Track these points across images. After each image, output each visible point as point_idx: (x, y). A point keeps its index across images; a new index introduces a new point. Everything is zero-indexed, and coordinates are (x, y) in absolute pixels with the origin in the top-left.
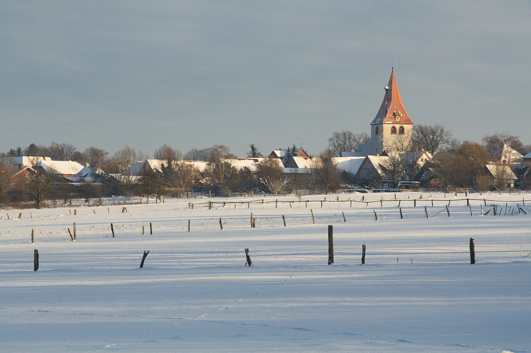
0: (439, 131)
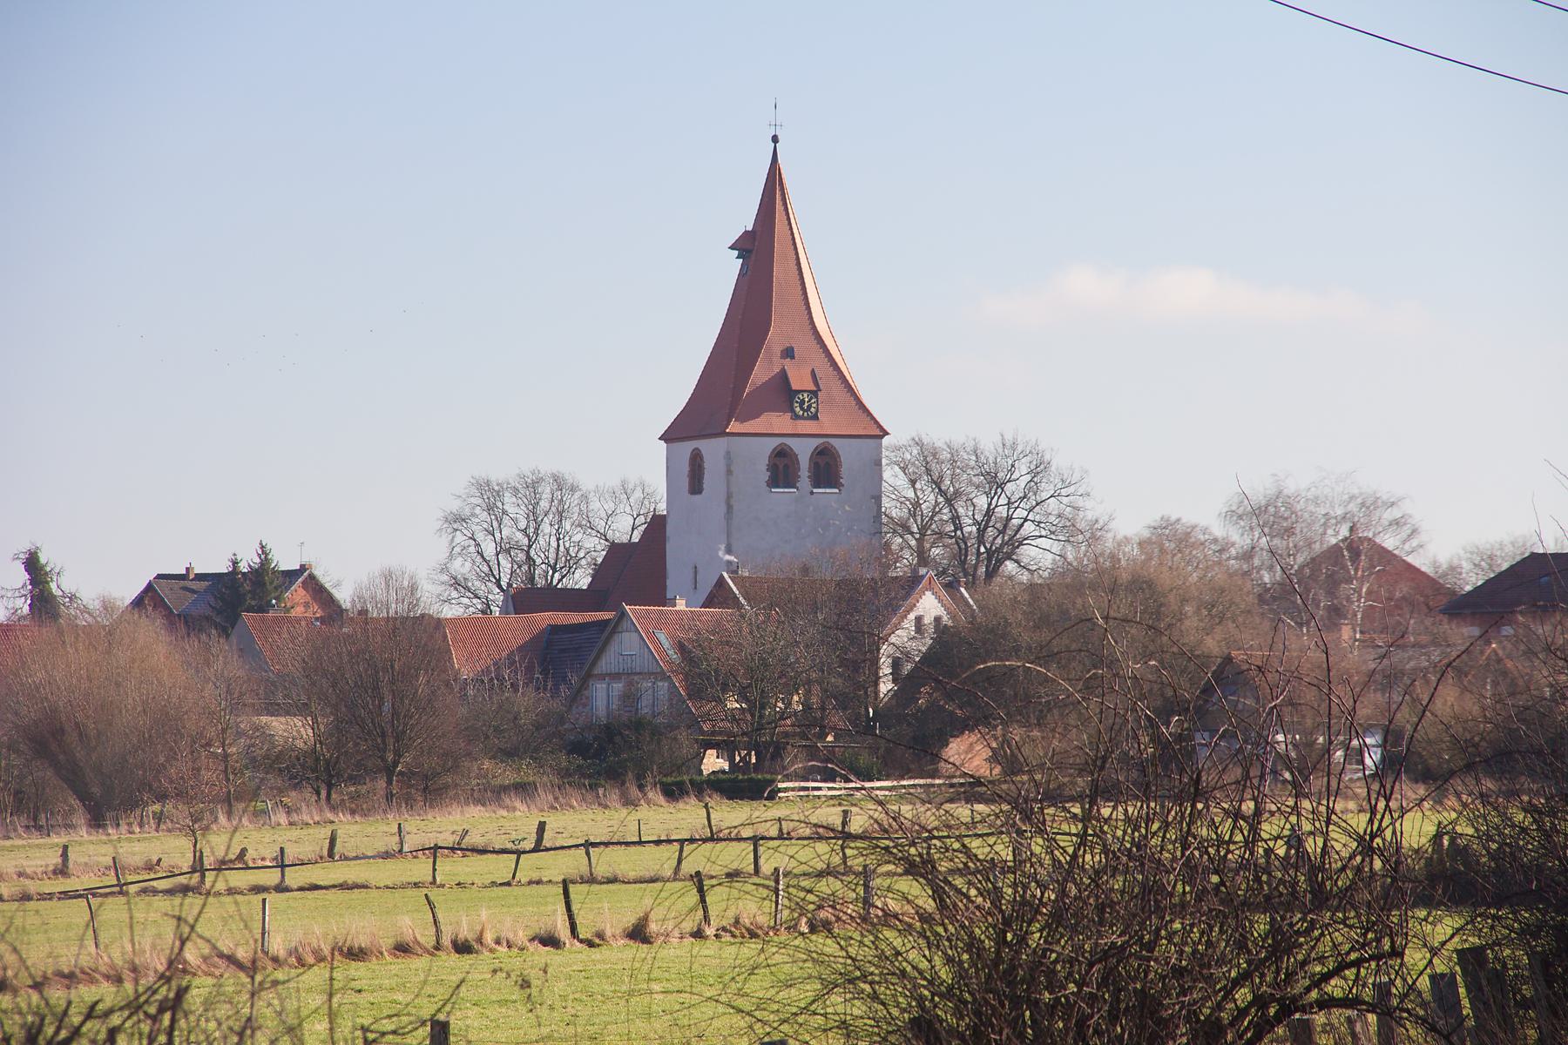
0: (1022, 468)
